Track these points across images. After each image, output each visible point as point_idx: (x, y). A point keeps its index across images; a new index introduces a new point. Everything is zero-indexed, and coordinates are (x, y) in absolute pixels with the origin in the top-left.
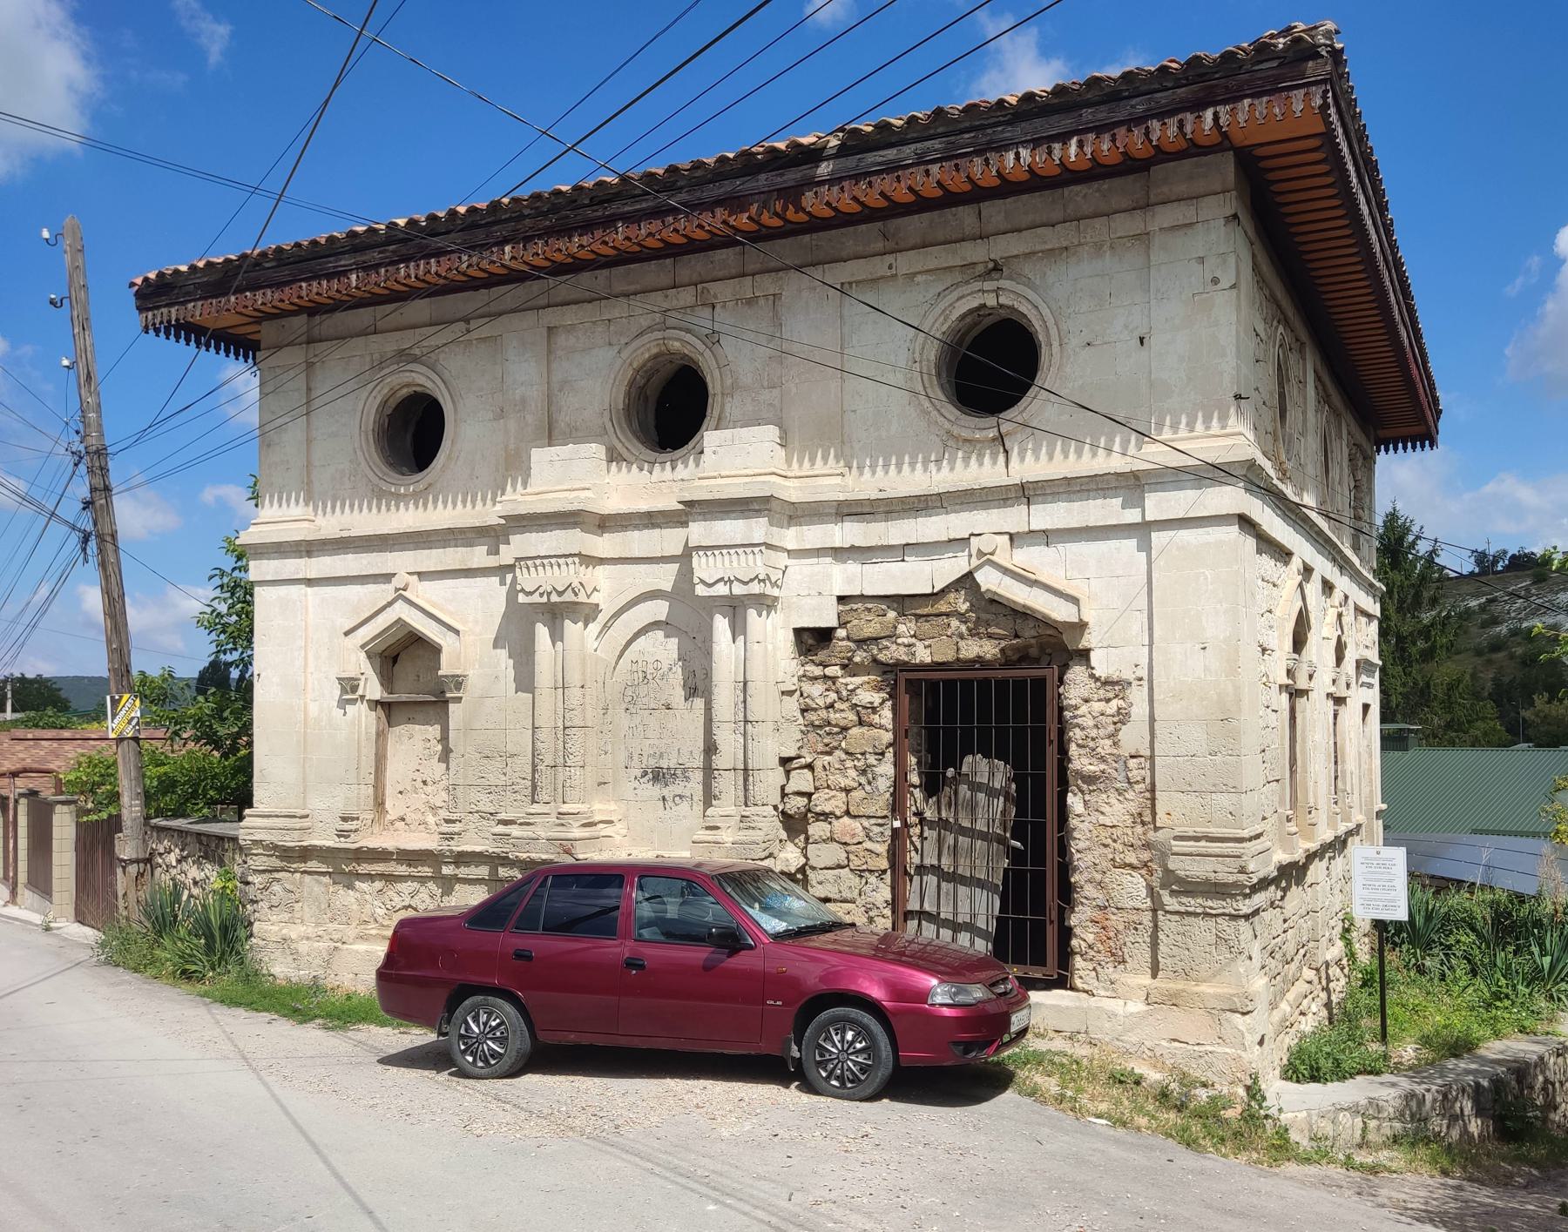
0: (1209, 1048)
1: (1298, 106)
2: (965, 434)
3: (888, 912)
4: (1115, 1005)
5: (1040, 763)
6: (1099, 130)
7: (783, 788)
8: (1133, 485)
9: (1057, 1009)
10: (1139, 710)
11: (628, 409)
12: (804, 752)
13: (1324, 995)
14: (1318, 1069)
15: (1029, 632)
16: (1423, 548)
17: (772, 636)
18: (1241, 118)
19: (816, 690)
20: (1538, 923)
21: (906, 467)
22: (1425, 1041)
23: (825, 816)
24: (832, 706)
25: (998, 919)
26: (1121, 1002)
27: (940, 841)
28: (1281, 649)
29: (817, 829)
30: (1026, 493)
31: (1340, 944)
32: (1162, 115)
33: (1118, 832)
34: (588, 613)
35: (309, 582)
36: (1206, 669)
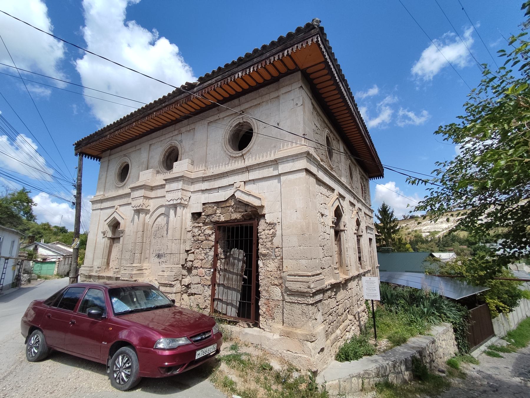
0: (300, 355)
1: (310, 43)
2: (234, 156)
3: (210, 298)
4: (269, 335)
5: (251, 251)
6: (258, 63)
7: (186, 259)
8: (275, 162)
9: (253, 335)
10: (278, 233)
11: (163, 162)
12: (192, 249)
13: (357, 323)
14: (348, 356)
15: (249, 210)
16: (390, 211)
17: (186, 214)
18: (294, 50)
19: (196, 230)
20: (422, 298)
21: (220, 167)
22: (389, 338)
23: (196, 268)
24: (199, 235)
25: (240, 302)
26: (272, 334)
27: (224, 276)
28: (330, 215)
29: (194, 272)
30: (248, 169)
31: (364, 305)
32: (273, 55)
33: (272, 273)
34: (147, 212)
35: (101, 209)
36: (297, 218)
